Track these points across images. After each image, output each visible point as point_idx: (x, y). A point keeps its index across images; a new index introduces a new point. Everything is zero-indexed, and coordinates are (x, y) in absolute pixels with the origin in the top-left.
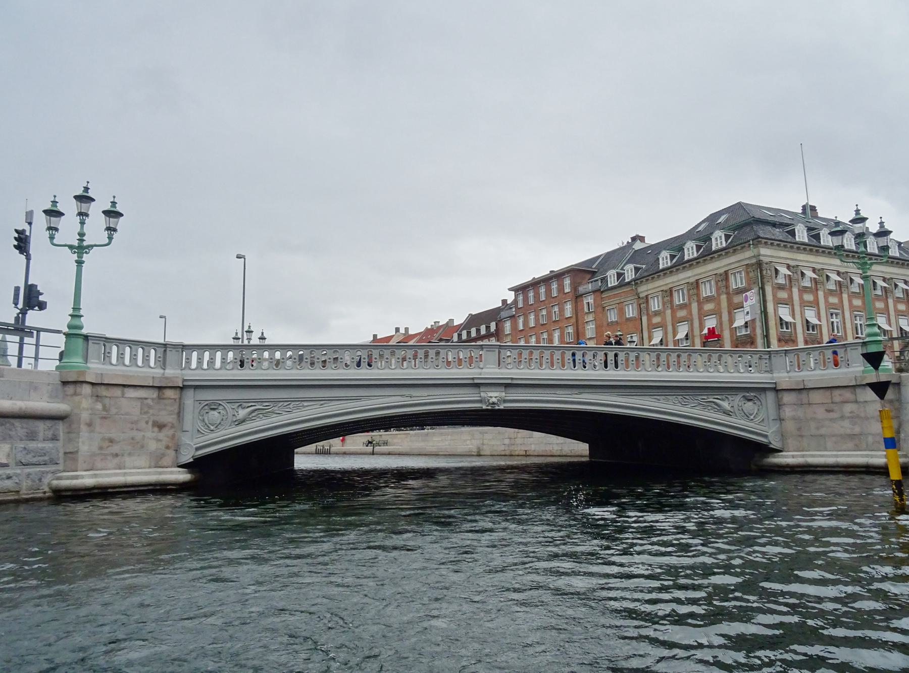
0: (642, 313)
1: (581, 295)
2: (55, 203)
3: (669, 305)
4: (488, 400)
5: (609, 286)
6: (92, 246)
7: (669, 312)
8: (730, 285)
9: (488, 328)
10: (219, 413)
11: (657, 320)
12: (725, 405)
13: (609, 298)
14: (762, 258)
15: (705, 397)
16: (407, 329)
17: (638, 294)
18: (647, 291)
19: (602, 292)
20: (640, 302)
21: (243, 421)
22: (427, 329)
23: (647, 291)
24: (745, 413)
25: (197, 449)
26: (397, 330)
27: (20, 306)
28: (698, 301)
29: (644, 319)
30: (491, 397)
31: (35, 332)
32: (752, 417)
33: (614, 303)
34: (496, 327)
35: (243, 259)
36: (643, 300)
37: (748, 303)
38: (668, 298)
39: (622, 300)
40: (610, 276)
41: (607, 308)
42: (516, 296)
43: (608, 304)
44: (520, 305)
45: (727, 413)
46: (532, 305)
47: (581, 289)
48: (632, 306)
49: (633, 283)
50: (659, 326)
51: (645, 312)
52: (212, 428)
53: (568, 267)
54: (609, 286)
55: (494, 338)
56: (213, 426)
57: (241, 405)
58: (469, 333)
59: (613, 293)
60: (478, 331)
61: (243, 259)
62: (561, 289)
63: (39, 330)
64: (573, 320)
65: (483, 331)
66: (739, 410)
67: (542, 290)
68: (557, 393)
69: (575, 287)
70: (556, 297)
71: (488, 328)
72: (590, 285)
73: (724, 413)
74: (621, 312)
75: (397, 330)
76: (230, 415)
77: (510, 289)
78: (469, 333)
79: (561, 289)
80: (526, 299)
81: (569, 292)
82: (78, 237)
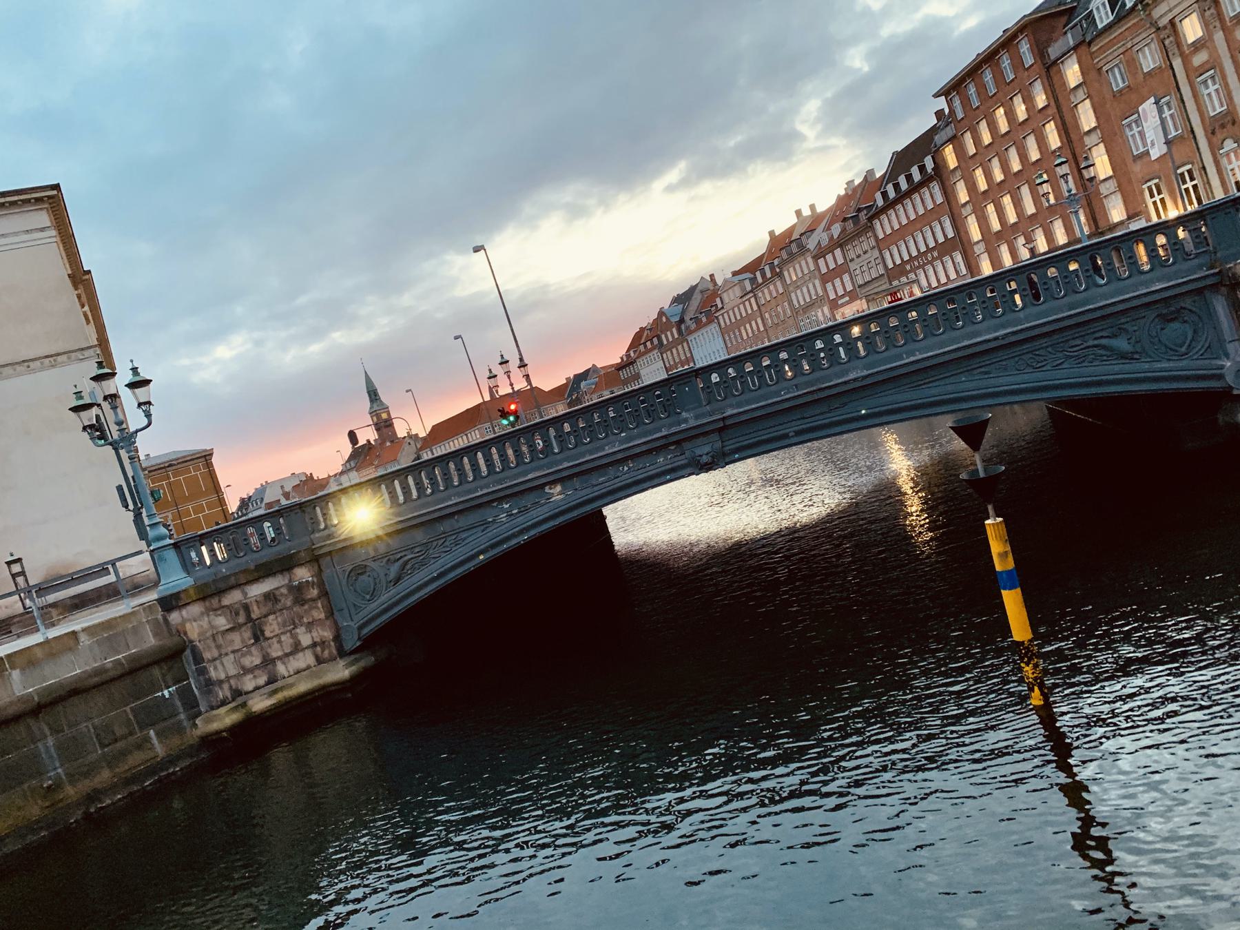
0: (1170, 54)
1: (1055, 62)
2: (79, 395)
3: (1218, 24)
4: (699, 461)
5: (1100, 26)
6: (137, 431)
7: (1219, 37)
8: (1225, 11)
9: (922, 169)
10: (369, 576)
11: (1199, 59)
12: (1122, 344)
15: (1078, 342)
16: (812, 207)
17: (1154, 24)
18: (1170, 10)
19: (1090, 44)
20: (1162, 36)
21: (398, 580)
22: (840, 199)
23: (1170, 10)
24: (1166, 346)
25: (360, 628)
26: (798, 213)
27: (131, 507)
28: (1223, 30)
29: (1177, 63)
30: (701, 456)
31: (110, 567)
32: (1183, 349)
33: (1116, 54)
34: (935, 163)
35: (483, 251)
36: (1167, 31)
37: (1149, 123)
38: (1212, 10)
39: (1129, 45)
40: (1098, 8)
41: (1105, 69)
42: (950, 103)
43: (1105, 61)
44: (960, 115)
45: (1123, 356)
46: (978, 108)
47: (1054, 51)
48: (1150, 49)
49: (1140, 7)
50: (1207, 67)
51: (1176, 51)
52: (368, 597)
53: (989, 47)
54: (1100, 26)
55: (935, 183)
56: (367, 594)
57: (389, 560)
58: (897, 186)
59: (1107, 40)
60: (909, 178)
61: (483, 251)
62: (1018, 63)
63: (113, 563)
64: (1053, 110)
65: (917, 176)
66: (1153, 344)
67: (1006, 62)
68: (805, 415)
69: (1040, 51)
70: (1013, 80)
71: (922, 169)
72: (1069, 35)
73: (1122, 358)
74: (1132, 65)
75: (798, 213)
76: (382, 575)
77: (937, 95)
78: (897, 186)
79: (1018, 63)
80: (966, 102)
81: (1032, 65)
82: (117, 428)
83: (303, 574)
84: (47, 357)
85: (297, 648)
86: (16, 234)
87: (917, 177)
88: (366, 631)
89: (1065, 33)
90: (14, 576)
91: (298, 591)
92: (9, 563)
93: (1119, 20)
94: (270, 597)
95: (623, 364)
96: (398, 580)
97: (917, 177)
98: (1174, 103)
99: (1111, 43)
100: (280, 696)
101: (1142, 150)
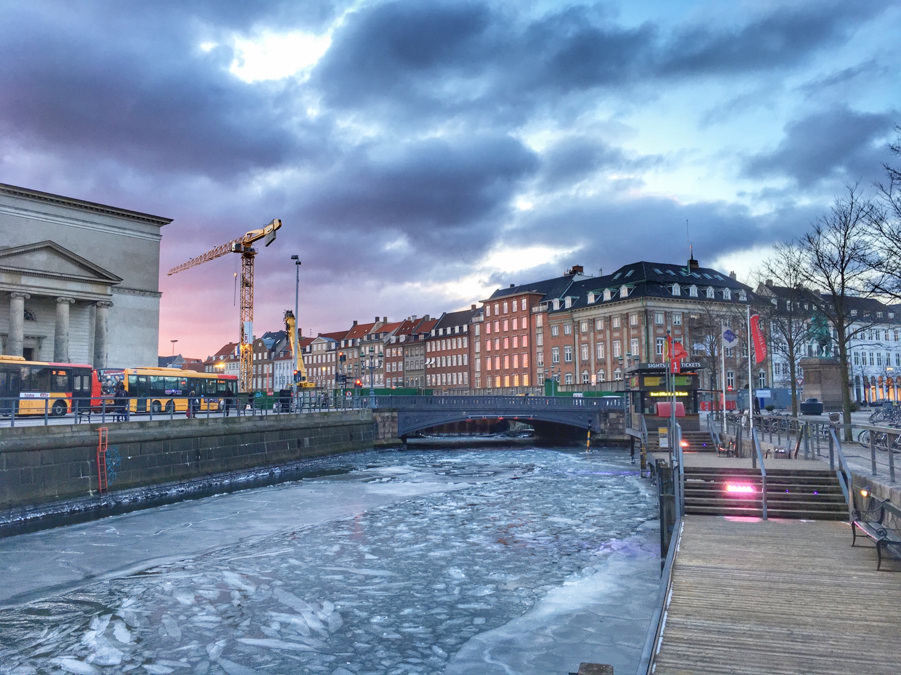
12: (581, 417)
13: (554, 319)
14: (648, 308)
17: (573, 319)
29: (577, 336)
94: (388, 417)
99: (557, 318)
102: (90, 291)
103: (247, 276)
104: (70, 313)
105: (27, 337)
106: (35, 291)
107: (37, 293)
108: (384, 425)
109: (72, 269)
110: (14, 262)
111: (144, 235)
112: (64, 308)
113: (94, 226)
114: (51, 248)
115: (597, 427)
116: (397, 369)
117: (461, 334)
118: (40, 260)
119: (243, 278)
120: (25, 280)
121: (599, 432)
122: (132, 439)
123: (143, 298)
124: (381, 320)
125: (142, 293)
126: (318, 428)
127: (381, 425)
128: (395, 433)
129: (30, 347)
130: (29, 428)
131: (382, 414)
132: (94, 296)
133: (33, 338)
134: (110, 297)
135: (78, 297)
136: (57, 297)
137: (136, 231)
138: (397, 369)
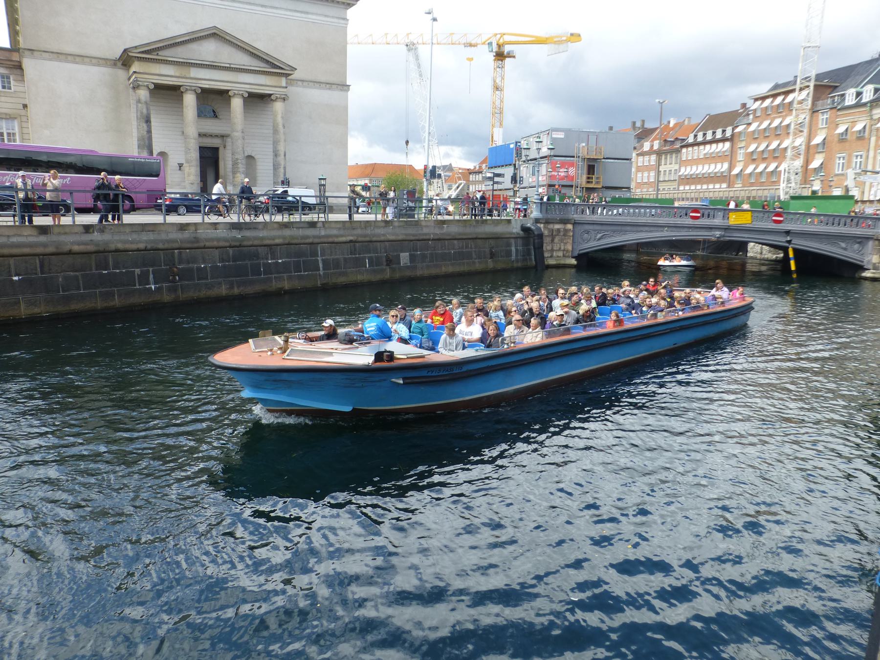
21: (599, 239)
83: (570, 227)
84: (311, 82)
85: (560, 250)
86: (333, 17)
87: (719, 135)
88: (581, 252)
89: (828, 98)
90: (321, 185)
91: (566, 231)
92: (320, 179)
93: (858, 105)
94: (558, 230)
95: (474, 171)
96: (599, 239)
97: (719, 135)
98: (864, 157)
99: (846, 115)
100: (558, 262)
101: (840, 172)
102: (264, 83)
103: (498, 80)
104: (244, 109)
105: (201, 135)
106: (206, 85)
107: (207, 86)
108: (553, 241)
109: (242, 60)
110: (180, 53)
111: (328, 19)
112: (237, 104)
113: (274, 11)
114: (216, 35)
115: (866, 259)
116: (649, 179)
117: (723, 140)
118: (208, 50)
119: (495, 81)
120: (195, 73)
121: (870, 267)
122: (215, 244)
123: (329, 92)
124: (638, 124)
125: (328, 86)
126: (429, 240)
127: (547, 240)
128: (567, 251)
129: (215, 146)
130: (188, 225)
131: (551, 226)
132: (268, 88)
133: (217, 136)
134: (285, 90)
135: (250, 90)
136: (228, 91)
137: (320, 15)
138: (649, 179)
